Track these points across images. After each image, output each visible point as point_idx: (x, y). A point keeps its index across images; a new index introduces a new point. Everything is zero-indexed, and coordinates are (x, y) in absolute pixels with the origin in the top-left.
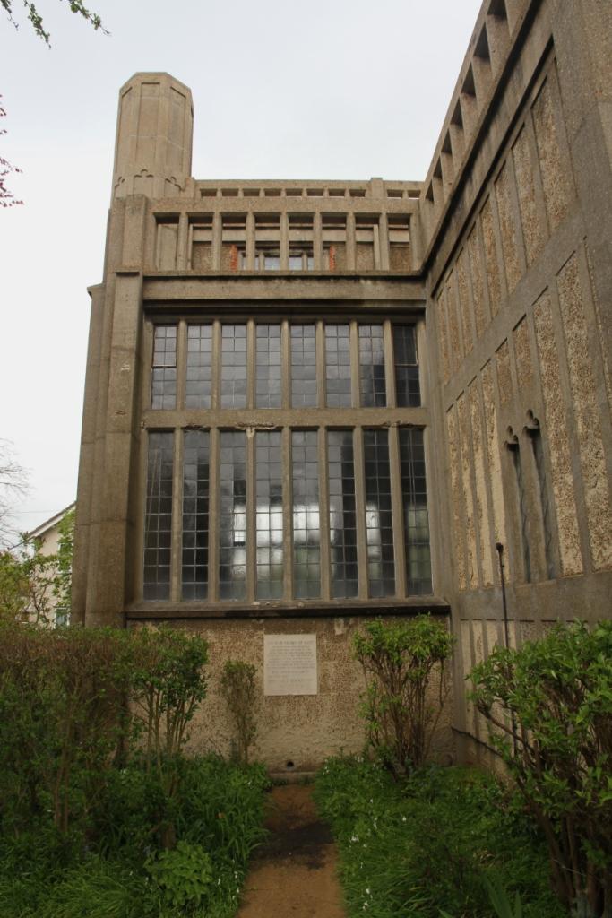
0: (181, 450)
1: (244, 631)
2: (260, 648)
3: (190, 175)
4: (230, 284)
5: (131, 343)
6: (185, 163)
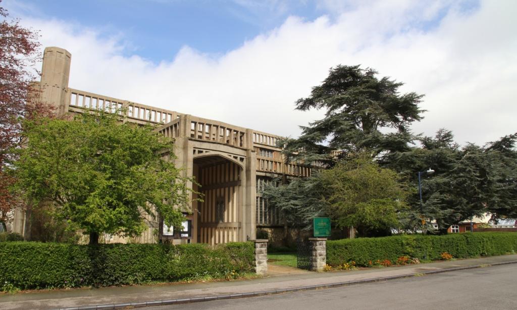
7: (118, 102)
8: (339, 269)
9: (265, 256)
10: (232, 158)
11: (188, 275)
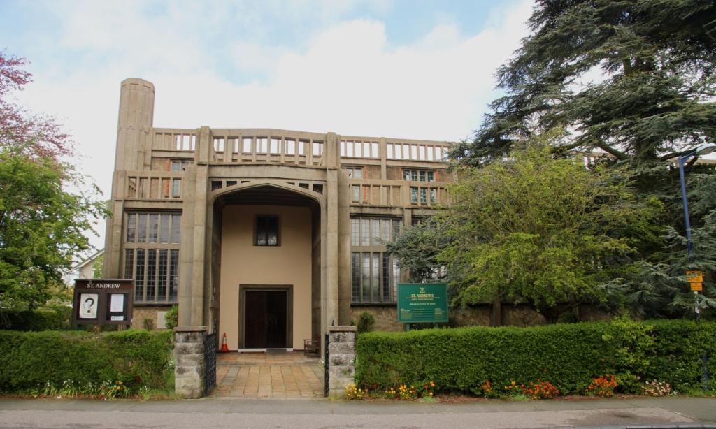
0: (110, 331)
1: (152, 310)
2: (157, 315)
3: (152, 125)
4: (153, 203)
5: (120, 223)
6: (149, 120)
7: (254, 134)
8: (389, 397)
9: (194, 359)
10: (296, 188)
11: (33, 384)
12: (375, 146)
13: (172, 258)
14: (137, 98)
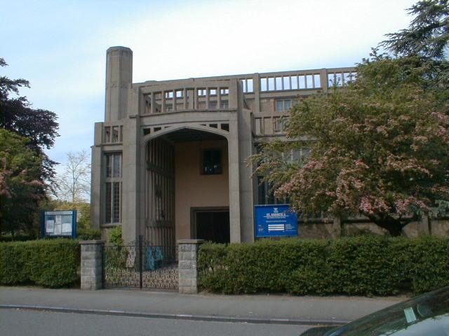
12: (317, 77)
13: (115, 189)
14: (121, 59)
